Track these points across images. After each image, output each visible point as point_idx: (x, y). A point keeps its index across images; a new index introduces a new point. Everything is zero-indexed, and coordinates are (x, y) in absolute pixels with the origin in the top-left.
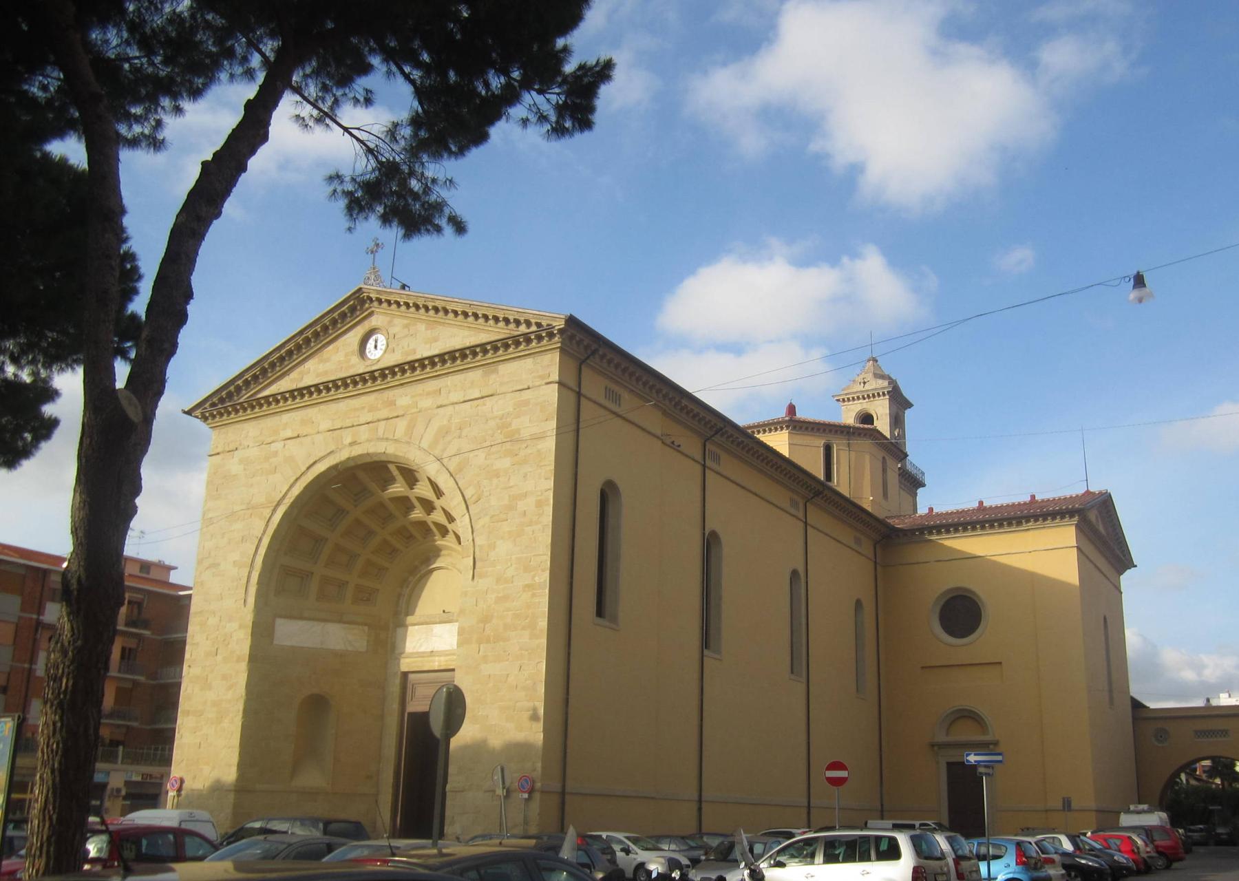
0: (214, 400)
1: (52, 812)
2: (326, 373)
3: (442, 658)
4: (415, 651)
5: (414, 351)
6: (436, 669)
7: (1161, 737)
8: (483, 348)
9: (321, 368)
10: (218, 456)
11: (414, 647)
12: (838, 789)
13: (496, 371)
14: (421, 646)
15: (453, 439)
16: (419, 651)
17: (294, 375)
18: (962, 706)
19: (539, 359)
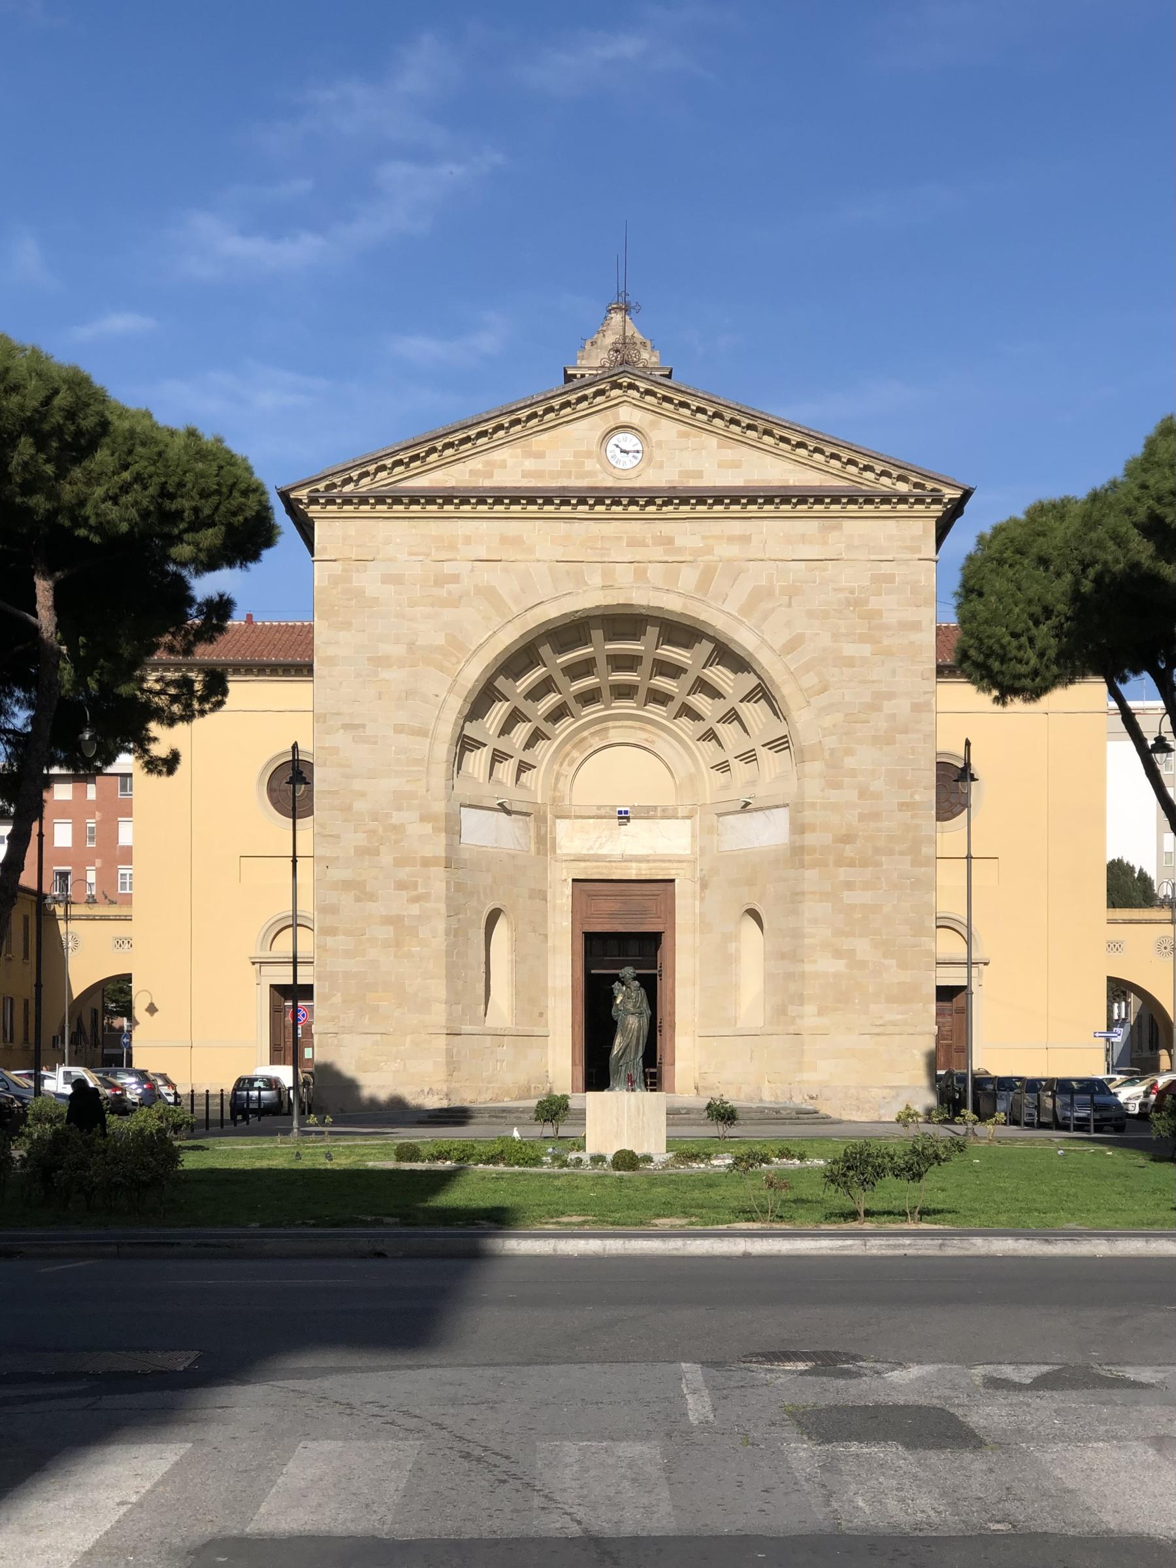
0: (335, 481)
1: (623, 1068)
2: (539, 474)
3: (643, 865)
4: (592, 852)
5: (699, 474)
6: (634, 878)
7: (1165, 948)
8: (819, 497)
9: (529, 464)
10: (972, 747)
11: (591, 848)
12: (44, 1050)
13: (840, 528)
14: (601, 846)
15: (778, 606)
16: (600, 852)
17: (476, 464)
18: (597, 858)
19: (904, 523)
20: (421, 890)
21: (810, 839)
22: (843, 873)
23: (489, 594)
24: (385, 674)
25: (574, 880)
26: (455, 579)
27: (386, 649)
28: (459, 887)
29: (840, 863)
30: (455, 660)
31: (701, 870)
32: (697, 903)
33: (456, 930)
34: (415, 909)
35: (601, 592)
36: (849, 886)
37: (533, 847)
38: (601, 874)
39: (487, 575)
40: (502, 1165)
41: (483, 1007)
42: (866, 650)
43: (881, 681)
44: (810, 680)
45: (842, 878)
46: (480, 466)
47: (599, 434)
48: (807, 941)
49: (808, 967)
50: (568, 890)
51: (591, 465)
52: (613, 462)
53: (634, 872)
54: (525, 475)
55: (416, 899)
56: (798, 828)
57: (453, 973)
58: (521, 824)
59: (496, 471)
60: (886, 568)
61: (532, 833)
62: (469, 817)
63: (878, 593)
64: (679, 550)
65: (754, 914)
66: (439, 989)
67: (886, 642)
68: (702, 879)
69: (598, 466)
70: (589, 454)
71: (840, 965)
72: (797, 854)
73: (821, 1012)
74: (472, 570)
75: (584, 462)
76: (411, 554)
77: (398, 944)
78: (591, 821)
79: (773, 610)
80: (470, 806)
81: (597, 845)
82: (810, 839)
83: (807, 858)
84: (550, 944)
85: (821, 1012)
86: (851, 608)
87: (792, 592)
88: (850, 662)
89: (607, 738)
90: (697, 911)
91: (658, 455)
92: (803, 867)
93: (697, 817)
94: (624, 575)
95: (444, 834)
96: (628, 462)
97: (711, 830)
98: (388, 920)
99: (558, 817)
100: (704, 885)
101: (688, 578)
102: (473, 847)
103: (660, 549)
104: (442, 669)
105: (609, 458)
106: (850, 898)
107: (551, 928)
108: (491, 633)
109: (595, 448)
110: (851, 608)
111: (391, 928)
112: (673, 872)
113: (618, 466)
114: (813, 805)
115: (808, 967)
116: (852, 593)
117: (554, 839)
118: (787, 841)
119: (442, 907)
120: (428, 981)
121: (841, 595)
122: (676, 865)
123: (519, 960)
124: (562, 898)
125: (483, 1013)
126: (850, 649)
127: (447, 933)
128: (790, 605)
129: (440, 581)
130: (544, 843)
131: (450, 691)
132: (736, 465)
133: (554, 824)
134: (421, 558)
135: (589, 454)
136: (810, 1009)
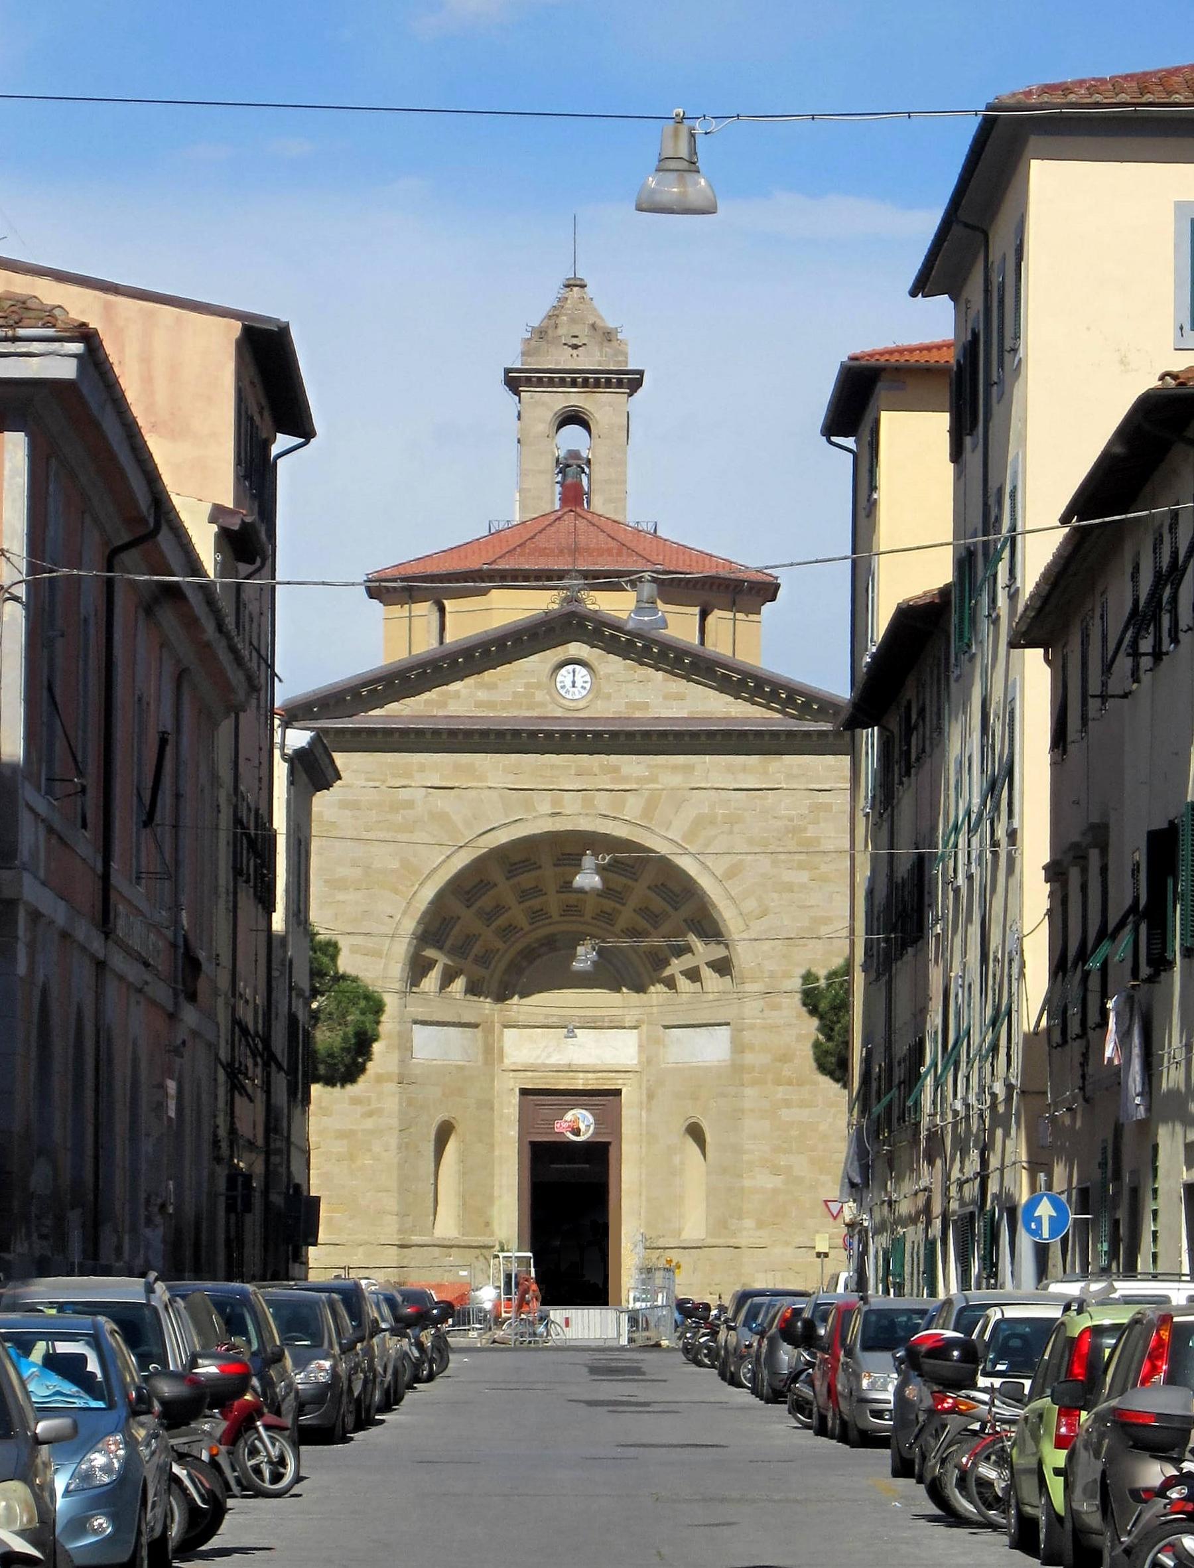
2: (491, 705)
4: (539, 1061)
5: (646, 706)
9: (482, 695)
11: (538, 1057)
14: (549, 1056)
20: (374, 1106)
21: (749, 1058)
22: (781, 1092)
23: (441, 818)
24: (341, 896)
25: (524, 1092)
26: (410, 804)
27: (343, 871)
28: (410, 1102)
29: (778, 1082)
30: (409, 883)
31: (648, 1081)
32: (644, 1114)
33: (407, 1144)
34: (369, 1124)
35: (550, 820)
36: (787, 1104)
37: (480, 1057)
38: (548, 1084)
39: (441, 801)
40: (185, 1472)
41: (432, 1218)
42: (803, 877)
43: (818, 906)
44: (750, 905)
45: (780, 1096)
46: (434, 696)
47: (549, 667)
48: (746, 1157)
49: (747, 1183)
50: (515, 1099)
51: (540, 696)
52: (562, 692)
53: (581, 1081)
54: (479, 704)
55: (370, 1114)
56: (738, 1047)
57: (404, 1189)
58: (469, 1035)
59: (450, 701)
60: (823, 798)
61: (480, 1043)
62: (420, 1034)
63: (816, 822)
64: (626, 779)
65: (696, 1133)
66: (391, 1203)
67: (824, 868)
68: (648, 1089)
69: (548, 697)
70: (539, 686)
71: (777, 1181)
72: (737, 1070)
73: (760, 1225)
74: (426, 796)
75: (534, 693)
76: (368, 780)
77: (352, 1158)
78: (539, 1030)
79: (715, 837)
80: (424, 1023)
81: (545, 1054)
82: (749, 1058)
83: (746, 1077)
84: (497, 1153)
85: (760, 1225)
86: (790, 835)
87: (732, 821)
88: (789, 888)
89: (469, 1313)
90: (644, 1120)
91: (607, 689)
92: (743, 1085)
93: (644, 1027)
94: (571, 803)
95: (397, 1051)
96: (577, 693)
97: (658, 1042)
98: (342, 1135)
99: (506, 1027)
100: (651, 1096)
101: (633, 807)
102: (422, 1061)
103: (607, 778)
104: (396, 891)
105: (559, 688)
106: (785, 1114)
107: (498, 1137)
108: (443, 857)
109: (545, 679)
110: (790, 835)
111: (345, 1142)
112: (620, 1081)
113: (567, 696)
114: (752, 1027)
115: (747, 1183)
116: (791, 820)
117: (501, 1049)
118: (728, 1058)
119: (394, 1122)
120: (380, 1194)
121: (779, 823)
122: (622, 1075)
123: (465, 1173)
124: (509, 1108)
125: (431, 1224)
126: (788, 876)
127: (399, 1148)
128: (731, 832)
129: (396, 807)
130: (492, 1053)
131: (404, 913)
132: (680, 697)
133: (502, 1033)
134: (377, 784)
135: (539, 686)
136: (749, 1223)
